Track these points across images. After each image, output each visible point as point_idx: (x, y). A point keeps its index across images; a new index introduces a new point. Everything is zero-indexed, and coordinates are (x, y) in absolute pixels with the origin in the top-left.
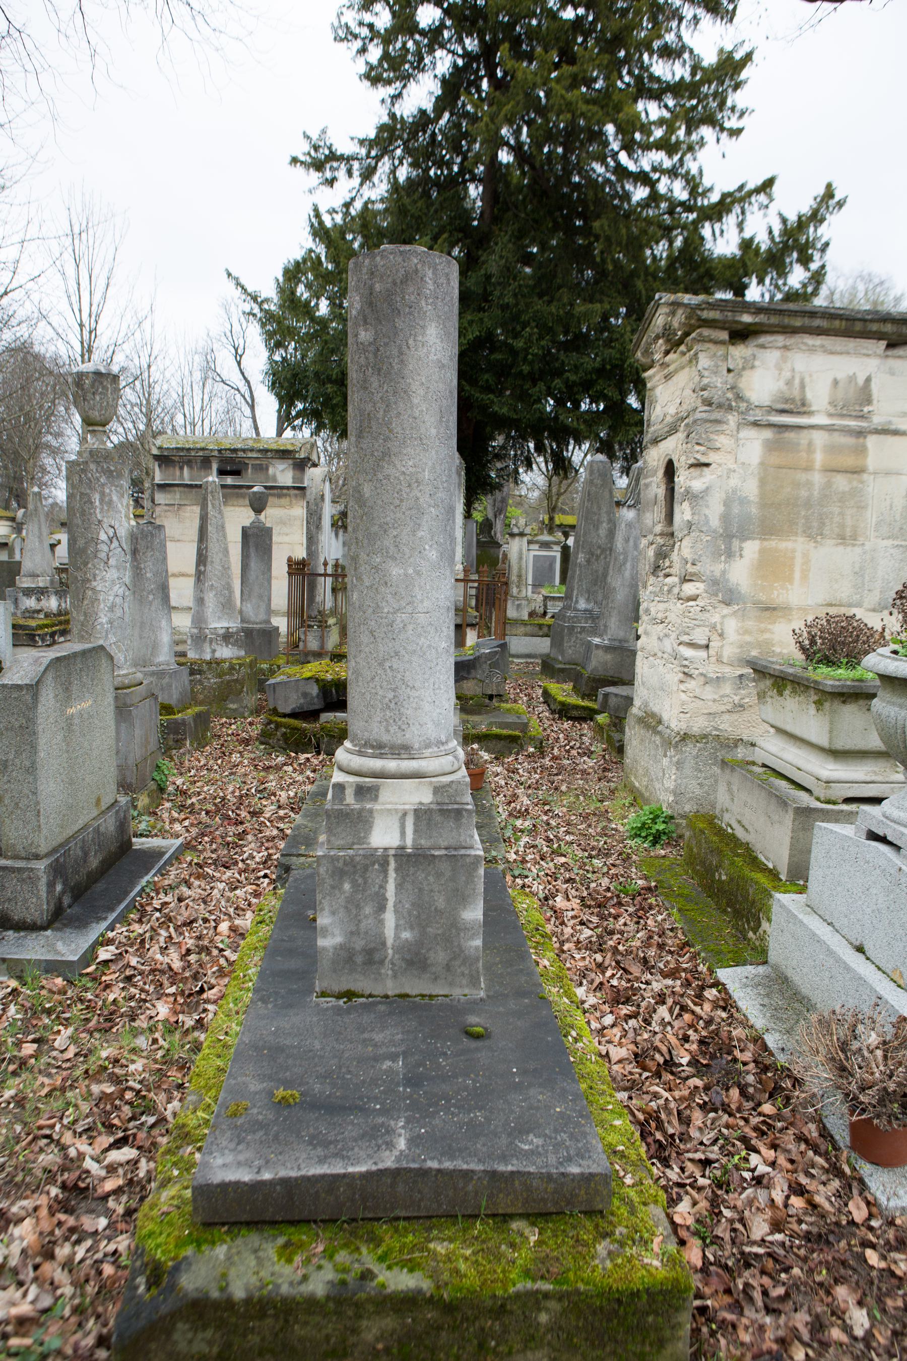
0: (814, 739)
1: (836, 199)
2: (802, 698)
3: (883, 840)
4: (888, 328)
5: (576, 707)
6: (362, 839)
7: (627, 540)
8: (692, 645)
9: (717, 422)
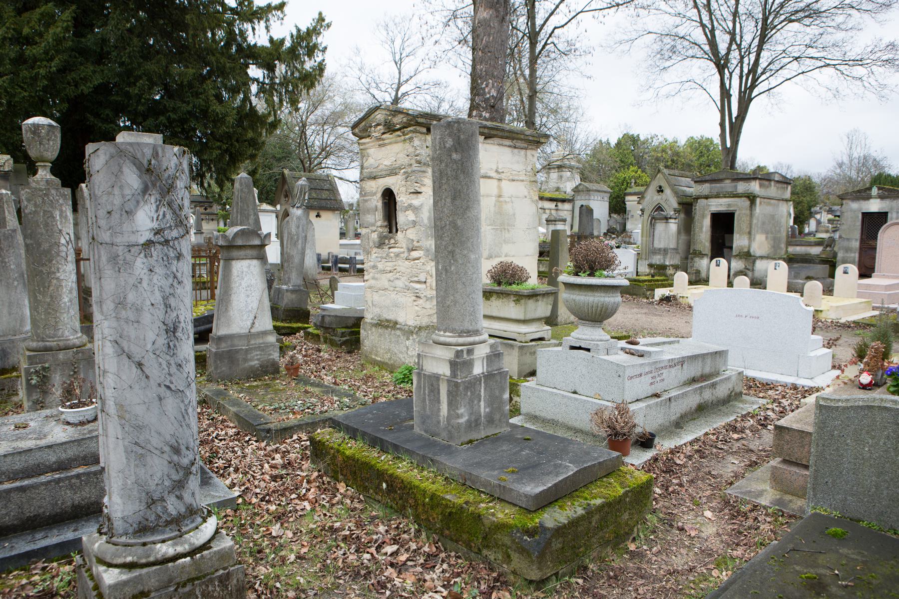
0: (513, 317)
1: (326, 22)
2: (505, 300)
3: (580, 348)
5: (284, 328)
6: (471, 372)
7: (298, 227)
8: (419, 282)
9: (424, 172)
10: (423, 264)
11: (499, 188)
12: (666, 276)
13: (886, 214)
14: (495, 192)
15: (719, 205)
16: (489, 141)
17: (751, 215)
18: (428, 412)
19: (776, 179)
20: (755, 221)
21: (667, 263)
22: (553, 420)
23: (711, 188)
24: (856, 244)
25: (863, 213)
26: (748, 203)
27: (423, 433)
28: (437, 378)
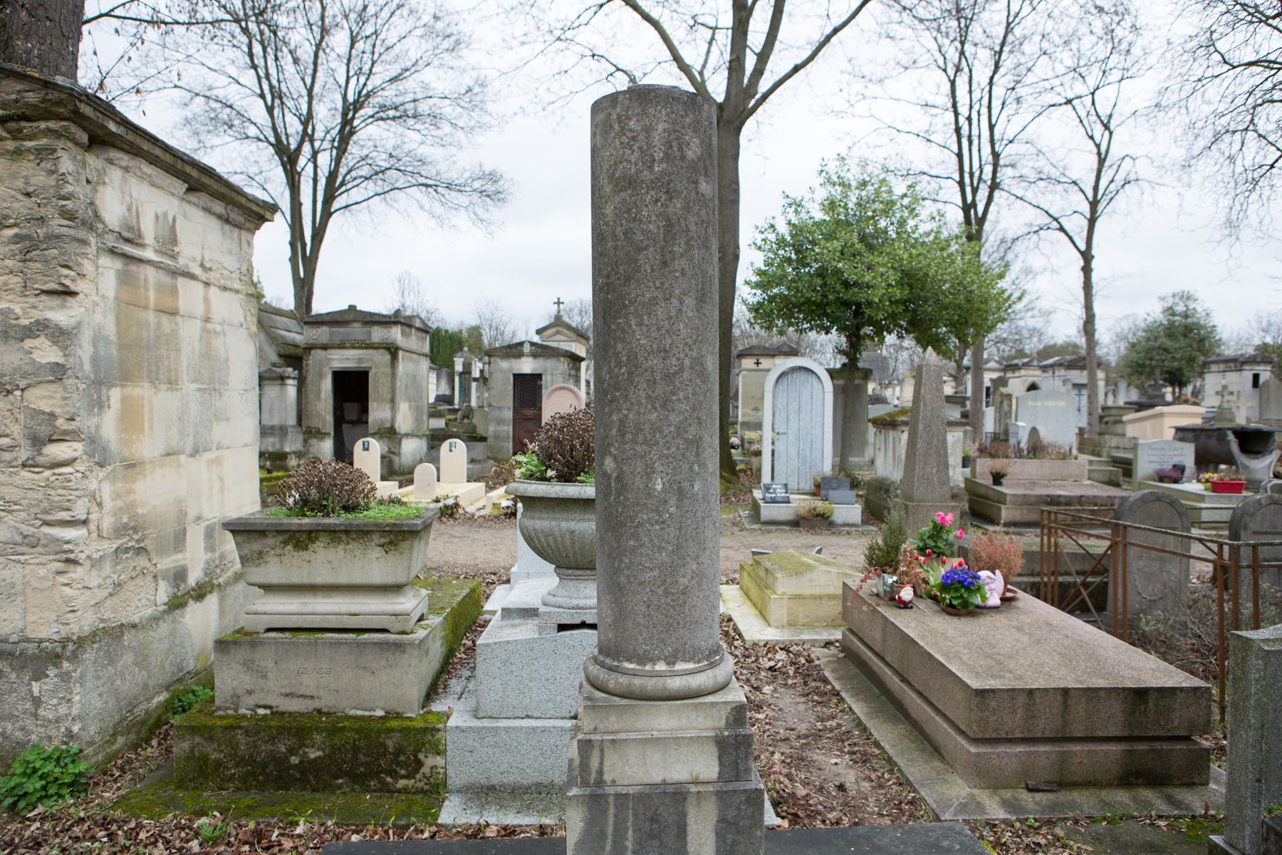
0: (377, 578)
4: (195, 173)
10: (85, 476)
11: (207, 300)
12: (287, 470)
13: (539, 376)
14: (200, 310)
15: (345, 359)
16: (192, 197)
17: (394, 375)
20: (398, 384)
21: (287, 449)
22: (538, 785)
23: (331, 334)
24: (509, 414)
25: (515, 375)
26: (388, 357)
28: (677, 795)
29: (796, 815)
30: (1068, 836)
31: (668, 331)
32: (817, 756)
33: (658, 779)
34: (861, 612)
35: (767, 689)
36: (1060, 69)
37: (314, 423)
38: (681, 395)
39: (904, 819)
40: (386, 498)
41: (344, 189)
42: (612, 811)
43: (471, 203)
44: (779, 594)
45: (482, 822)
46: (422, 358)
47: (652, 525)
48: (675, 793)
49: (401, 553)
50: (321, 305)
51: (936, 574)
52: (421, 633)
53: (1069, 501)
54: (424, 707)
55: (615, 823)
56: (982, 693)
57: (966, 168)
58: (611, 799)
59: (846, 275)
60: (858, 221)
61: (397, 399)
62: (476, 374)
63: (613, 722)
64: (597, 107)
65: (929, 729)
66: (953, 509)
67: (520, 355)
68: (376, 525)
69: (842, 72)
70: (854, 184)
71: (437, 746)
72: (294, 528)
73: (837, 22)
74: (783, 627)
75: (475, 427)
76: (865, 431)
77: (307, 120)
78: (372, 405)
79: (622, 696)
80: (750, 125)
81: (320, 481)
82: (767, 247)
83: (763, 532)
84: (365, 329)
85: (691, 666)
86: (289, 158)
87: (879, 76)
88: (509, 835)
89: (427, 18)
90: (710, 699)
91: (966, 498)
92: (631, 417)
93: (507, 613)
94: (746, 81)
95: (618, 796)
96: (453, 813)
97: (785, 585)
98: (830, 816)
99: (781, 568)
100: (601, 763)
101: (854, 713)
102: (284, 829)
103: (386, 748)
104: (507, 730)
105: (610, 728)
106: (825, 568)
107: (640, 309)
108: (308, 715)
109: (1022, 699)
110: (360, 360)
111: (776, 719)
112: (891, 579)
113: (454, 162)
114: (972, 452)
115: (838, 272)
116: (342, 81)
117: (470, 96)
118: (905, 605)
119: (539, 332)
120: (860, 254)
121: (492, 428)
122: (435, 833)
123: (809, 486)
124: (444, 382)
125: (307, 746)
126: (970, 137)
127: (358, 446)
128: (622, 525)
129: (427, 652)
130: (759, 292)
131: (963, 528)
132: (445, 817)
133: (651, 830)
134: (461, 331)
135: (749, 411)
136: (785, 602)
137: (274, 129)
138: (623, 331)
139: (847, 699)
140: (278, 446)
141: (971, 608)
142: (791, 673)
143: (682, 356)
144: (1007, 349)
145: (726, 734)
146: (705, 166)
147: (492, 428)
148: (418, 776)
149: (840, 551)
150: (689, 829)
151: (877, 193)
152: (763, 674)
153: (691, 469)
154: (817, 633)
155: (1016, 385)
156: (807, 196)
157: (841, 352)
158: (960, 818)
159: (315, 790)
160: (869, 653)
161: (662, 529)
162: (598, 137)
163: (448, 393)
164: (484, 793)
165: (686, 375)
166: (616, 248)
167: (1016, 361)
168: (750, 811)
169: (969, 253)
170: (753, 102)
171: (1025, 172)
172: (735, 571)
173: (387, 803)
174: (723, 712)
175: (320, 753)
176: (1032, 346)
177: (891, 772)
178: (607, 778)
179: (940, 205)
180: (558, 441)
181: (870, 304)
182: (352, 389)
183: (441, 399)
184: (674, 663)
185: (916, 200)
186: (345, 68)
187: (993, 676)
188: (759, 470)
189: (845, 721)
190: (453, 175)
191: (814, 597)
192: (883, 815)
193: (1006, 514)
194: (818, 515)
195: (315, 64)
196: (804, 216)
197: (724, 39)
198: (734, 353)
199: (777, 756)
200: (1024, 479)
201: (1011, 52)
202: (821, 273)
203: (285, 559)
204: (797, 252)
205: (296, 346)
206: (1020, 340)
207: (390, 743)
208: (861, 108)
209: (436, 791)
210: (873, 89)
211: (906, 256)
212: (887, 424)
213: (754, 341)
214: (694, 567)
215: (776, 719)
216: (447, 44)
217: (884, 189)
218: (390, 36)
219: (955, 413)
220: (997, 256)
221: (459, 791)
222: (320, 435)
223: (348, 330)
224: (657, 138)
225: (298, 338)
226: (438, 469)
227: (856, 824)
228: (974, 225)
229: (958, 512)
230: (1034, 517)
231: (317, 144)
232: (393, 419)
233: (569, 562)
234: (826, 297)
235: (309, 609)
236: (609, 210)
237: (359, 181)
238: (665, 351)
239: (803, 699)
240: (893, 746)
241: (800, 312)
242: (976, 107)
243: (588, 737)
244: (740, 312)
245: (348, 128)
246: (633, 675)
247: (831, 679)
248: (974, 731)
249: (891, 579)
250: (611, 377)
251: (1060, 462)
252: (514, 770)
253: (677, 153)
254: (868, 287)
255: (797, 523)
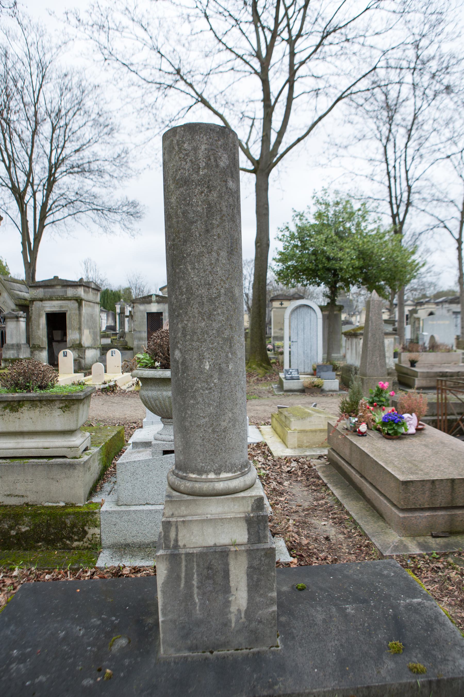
0: (59, 427)
15: (53, 306)
17: (80, 315)
18: (198, 613)
19: (93, 287)
20: (83, 319)
23: (45, 293)
24: (145, 335)
25: (147, 313)
26: (76, 305)
27: (186, 654)
28: (222, 553)
29: (301, 556)
30: (455, 563)
31: (210, 272)
32: (314, 521)
33: (211, 543)
34: (338, 439)
35: (286, 483)
36: (444, 139)
37: (37, 342)
38: (220, 311)
39: (363, 555)
40: (76, 382)
41: (51, 212)
42: (184, 563)
43: (122, 219)
44: (284, 429)
45: (121, 565)
46: (96, 305)
47: (204, 390)
48: (222, 552)
49: (72, 412)
50: (40, 277)
51: (379, 416)
52: (85, 458)
53: (452, 375)
54: (88, 500)
55: (186, 570)
56: (406, 483)
57: (393, 195)
58: (183, 557)
59: (328, 253)
60: (334, 224)
61: (83, 327)
62: (127, 313)
63: (183, 510)
64: (165, 137)
65: (376, 504)
66: (388, 380)
67: (150, 302)
68: (57, 396)
69: (325, 142)
70: (331, 204)
71: (95, 522)
72: (10, 400)
73: (320, 113)
74: (295, 448)
75: (126, 342)
76: (341, 339)
77: (29, 174)
78: (69, 332)
79: (188, 494)
80: (274, 171)
81: (25, 372)
82: (285, 239)
83: (285, 396)
84: (63, 289)
85: (230, 475)
86: (20, 195)
87: (345, 144)
88: (137, 572)
89: (93, 116)
90: (242, 494)
91: (396, 374)
92: (189, 325)
93: (136, 445)
94: (271, 147)
95: (187, 554)
96: (105, 560)
97: (296, 425)
98: (321, 555)
99: (294, 416)
100: (177, 535)
101: (335, 496)
102: (7, 573)
103: (66, 524)
104: (135, 512)
105: (182, 514)
106: (318, 415)
107: (193, 259)
108: (21, 507)
109: (428, 485)
110: (61, 307)
111: (291, 500)
112: (354, 420)
113: (112, 197)
114: (399, 349)
115: (323, 252)
116: (48, 152)
117: (120, 159)
118: (362, 434)
119: (161, 289)
120: (336, 242)
121: (136, 343)
122: (94, 573)
123: (310, 370)
124: (110, 319)
125: (20, 525)
126: (395, 177)
127: (61, 354)
128: (186, 391)
129: (89, 469)
130: (280, 264)
131: (395, 391)
132: (100, 563)
133: (208, 574)
134: (120, 291)
135: (277, 330)
136: (296, 435)
137: (11, 179)
138: (183, 273)
139: (331, 488)
140: (16, 355)
141: (399, 435)
142: (300, 474)
143: (219, 287)
144: (417, 293)
145: (252, 515)
146: (232, 172)
147: (136, 343)
148: (85, 540)
149: (327, 405)
150: (231, 573)
151: (345, 208)
152: (284, 475)
153: (227, 356)
154: (314, 451)
155: (422, 313)
156: (306, 211)
157: (327, 296)
158: (395, 554)
159: (25, 550)
160: (343, 462)
161: (210, 393)
162: (166, 155)
163: (113, 324)
164: (123, 548)
165: (222, 299)
166: (178, 222)
167: (422, 300)
168: (267, 561)
169: (396, 240)
170: (275, 159)
171: (425, 196)
172: (269, 418)
173: (67, 555)
174: (250, 502)
175: (28, 528)
176: (430, 292)
177: (355, 528)
178: (181, 543)
179: (379, 215)
180: (160, 346)
181: (341, 269)
182: (57, 322)
183: (108, 328)
184: (220, 474)
185: (366, 212)
186: (49, 145)
187: (412, 473)
188: (283, 362)
189: (330, 501)
190: (112, 204)
191: (312, 431)
192: (351, 554)
193: (418, 382)
194: (315, 386)
195: (33, 143)
196: (304, 221)
197: (259, 124)
198: (268, 298)
199: (291, 522)
200: (427, 363)
201: (417, 129)
202: (315, 253)
203: (6, 418)
204: (302, 242)
205: (26, 300)
206: (424, 289)
207: (68, 522)
208: (335, 162)
209: (95, 548)
210: (342, 152)
211: (361, 242)
212: (352, 335)
213: (280, 292)
214: (230, 415)
215: (291, 500)
216: (106, 130)
217: (348, 206)
218: (74, 126)
219: (389, 329)
220: (410, 243)
221: (109, 548)
222: (40, 348)
223: (54, 290)
224: (201, 154)
225: (27, 295)
226: (105, 366)
227: (336, 560)
228: (398, 228)
229: (391, 382)
230: (433, 384)
231: (35, 187)
232: (80, 339)
233: (165, 415)
234: (317, 266)
235: (20, 446)
236: (173, 200)
237: (60, 207)
238: (209, 284)
239: (306, 489)
240: (357, 514)
241: (303, 275)
242: (398, 161)
243: (168, 519)
244: (271, 276)
245: (52, 178)
246: (195, 481)
247: (322, 477)
248: (402, 504)
249: (354, 420)
250: (177, 302)
251: (447, 354)
252: (140, 534)
253: (214, 163)
254: (341, 260)
255: (303, 391)
